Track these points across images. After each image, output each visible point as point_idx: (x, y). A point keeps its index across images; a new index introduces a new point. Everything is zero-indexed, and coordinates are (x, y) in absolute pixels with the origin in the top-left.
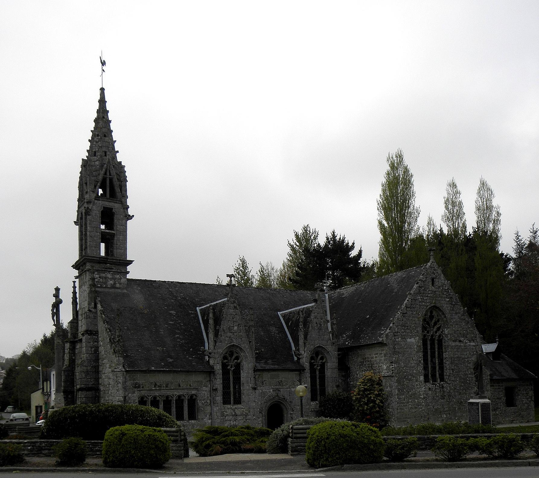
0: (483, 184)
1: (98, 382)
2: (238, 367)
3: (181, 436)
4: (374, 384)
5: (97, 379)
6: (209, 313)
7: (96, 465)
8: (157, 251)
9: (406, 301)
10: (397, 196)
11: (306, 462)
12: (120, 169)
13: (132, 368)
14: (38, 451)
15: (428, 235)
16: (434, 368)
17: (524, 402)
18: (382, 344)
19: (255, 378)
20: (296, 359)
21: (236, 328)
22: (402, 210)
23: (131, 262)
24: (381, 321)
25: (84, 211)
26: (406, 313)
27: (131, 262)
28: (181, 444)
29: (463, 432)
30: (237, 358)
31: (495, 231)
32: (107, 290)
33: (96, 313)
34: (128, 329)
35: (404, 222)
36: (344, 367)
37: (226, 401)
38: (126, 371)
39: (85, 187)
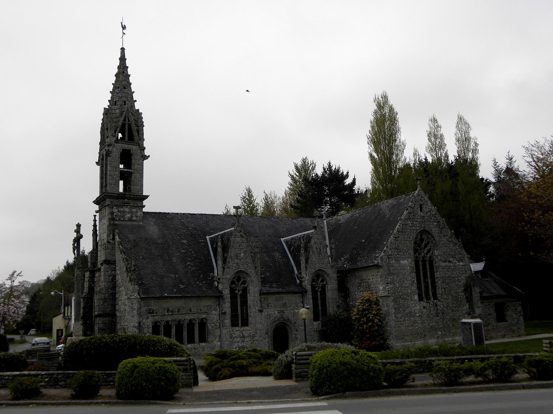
0: (461, 119)
1: (115, 308)
2: (245, 291)
3: (190, 364)
4: (372, 304)
5: (114, 306)
6: (217, 242)
7: (110, 396)
8: (171, 186)
9: (398, 226)
10: (384, 130)
11: (309, 389)
12: (138, 115)
13: (146, 295)
14: (54, 383)
15: (414, 164)
16: (427, 287)
17: (514, 317)
18: (377, 266)
19: (261, 301)
20: (298, 281)
21: (242, 255)
22: (389, 143)
23: (147, 197)
24: (374, 243)
25: (105, 153)
27: (147, 197)
28: (191, 373)
29: (458, 354)
30: (244, 283)
31: (474, 160)
32: (124, 223)
33: (114, 244)
34: (143, 258)
35: (391, 154)
36: (343, 289)
37: (234, 324)
38: (141, 298)
39: (106, 132)
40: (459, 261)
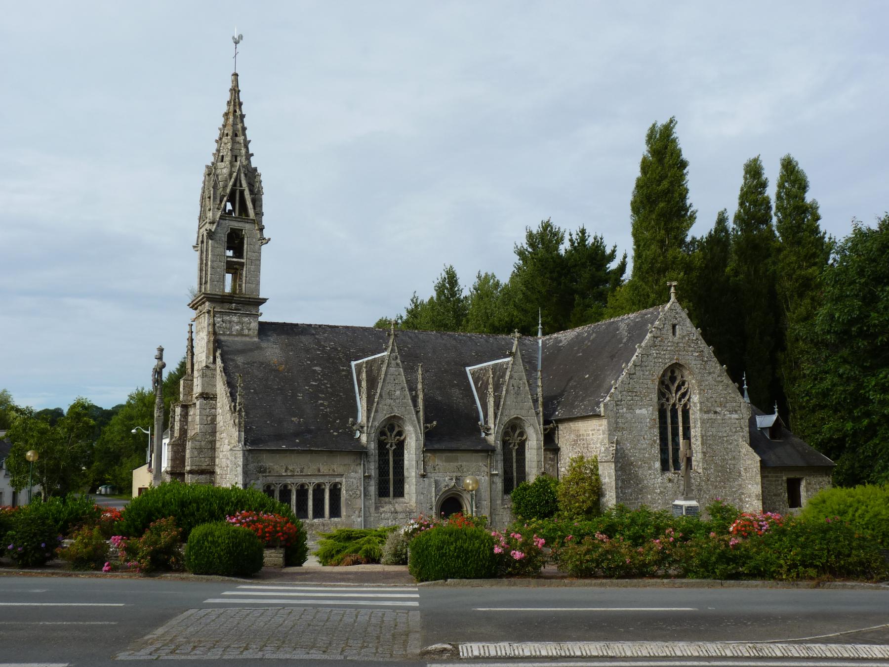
2: (401, 445)
5: (213, 459)
9: (634, 357)
12: (252, 175)
21: (398, 393)
23: (264, 301)
26: (634, 374)
27: (264, 301)
30: (400, 433)
32: (231, 339)
33: (215, 370)
39: (207, 202)
40: (731, 412)
